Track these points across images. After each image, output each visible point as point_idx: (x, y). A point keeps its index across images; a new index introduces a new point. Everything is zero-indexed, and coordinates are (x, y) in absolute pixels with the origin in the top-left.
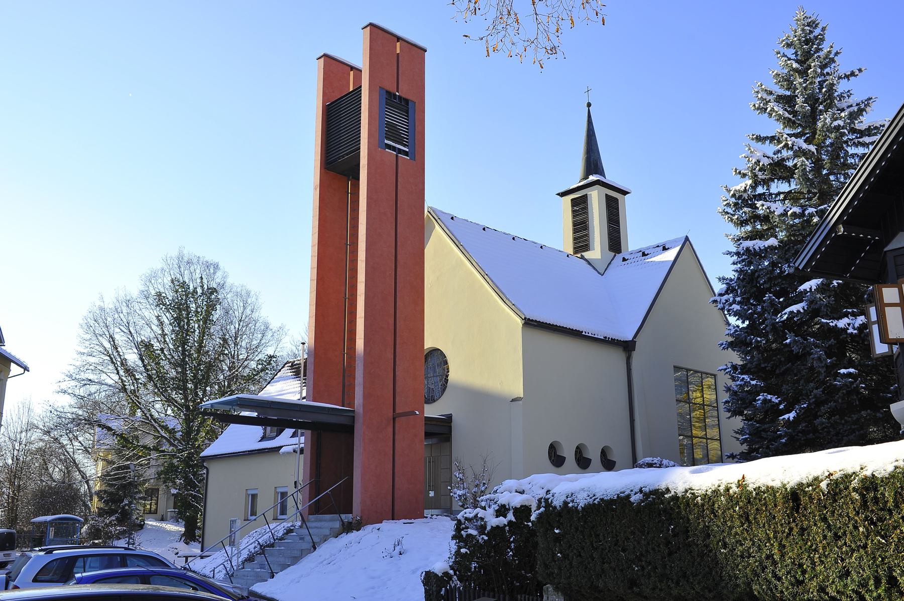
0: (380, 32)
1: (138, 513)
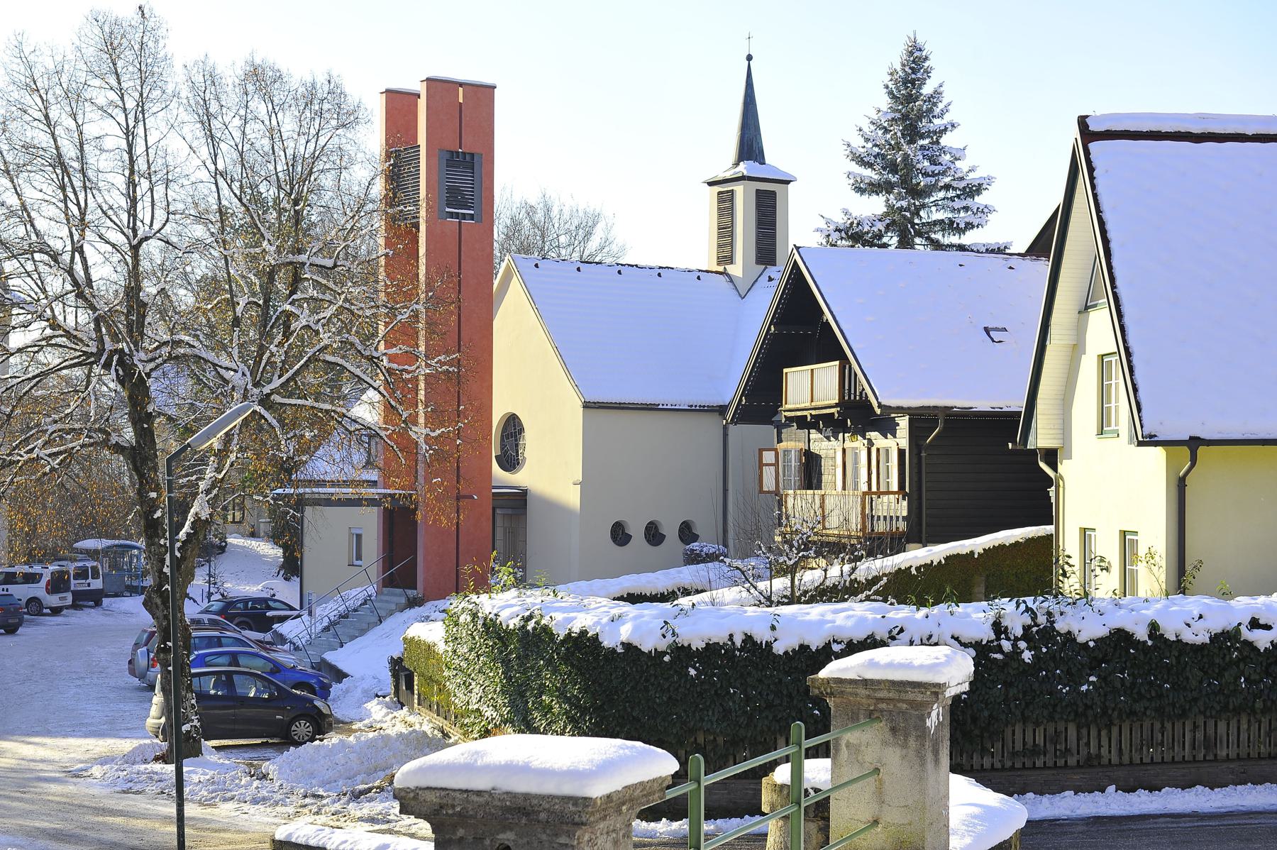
0: (438, 83)
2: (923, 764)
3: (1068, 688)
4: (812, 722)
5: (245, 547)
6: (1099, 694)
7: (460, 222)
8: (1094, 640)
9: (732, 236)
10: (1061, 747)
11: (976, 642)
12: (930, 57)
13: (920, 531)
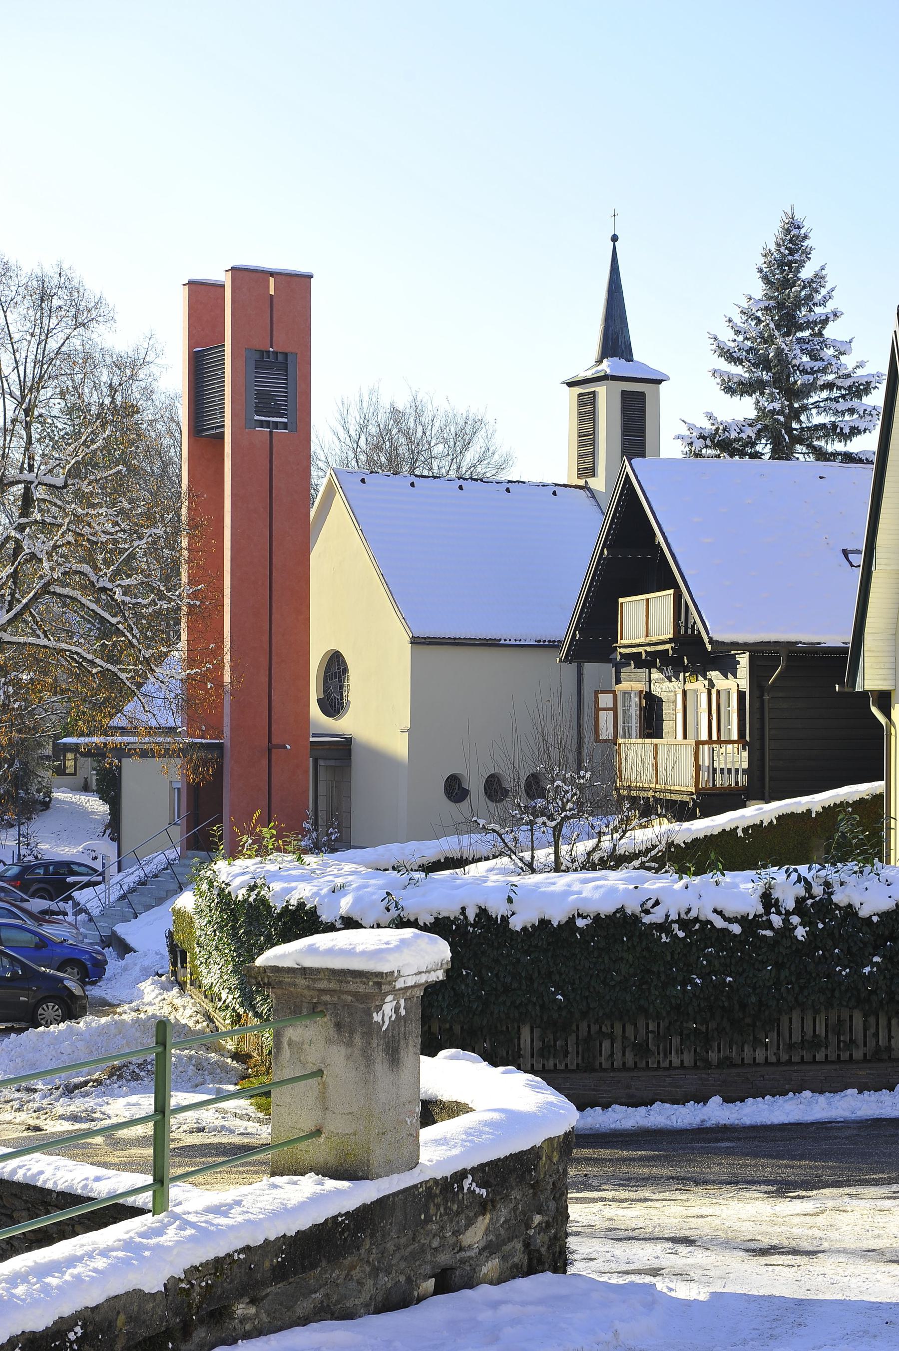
1: (39, 782)
2: (369, 1061)
3: (848, 970)
4: (556, 1008)
5: (72, 802)
6: (885, 977)
7: (271, 432)
8: (878, 915)
9: (594, 444)
10: (845, 1038)
11: (742, 916)
12: (810, 235)
13: (763, 787)
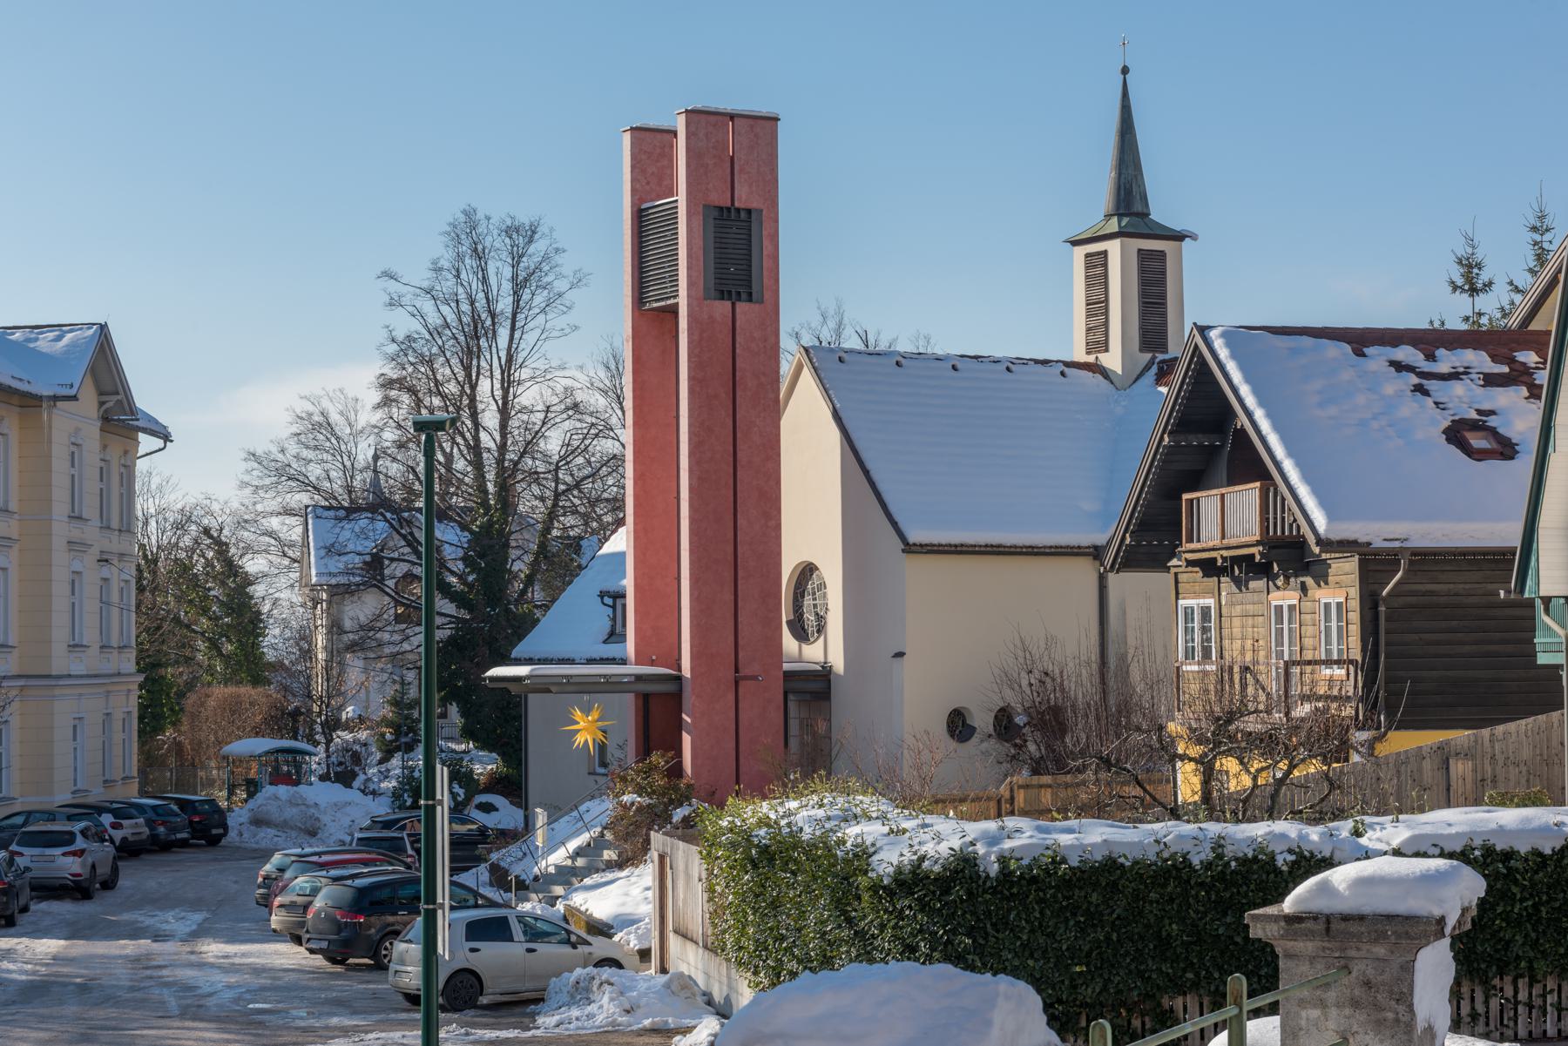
9: (1106, 313)
